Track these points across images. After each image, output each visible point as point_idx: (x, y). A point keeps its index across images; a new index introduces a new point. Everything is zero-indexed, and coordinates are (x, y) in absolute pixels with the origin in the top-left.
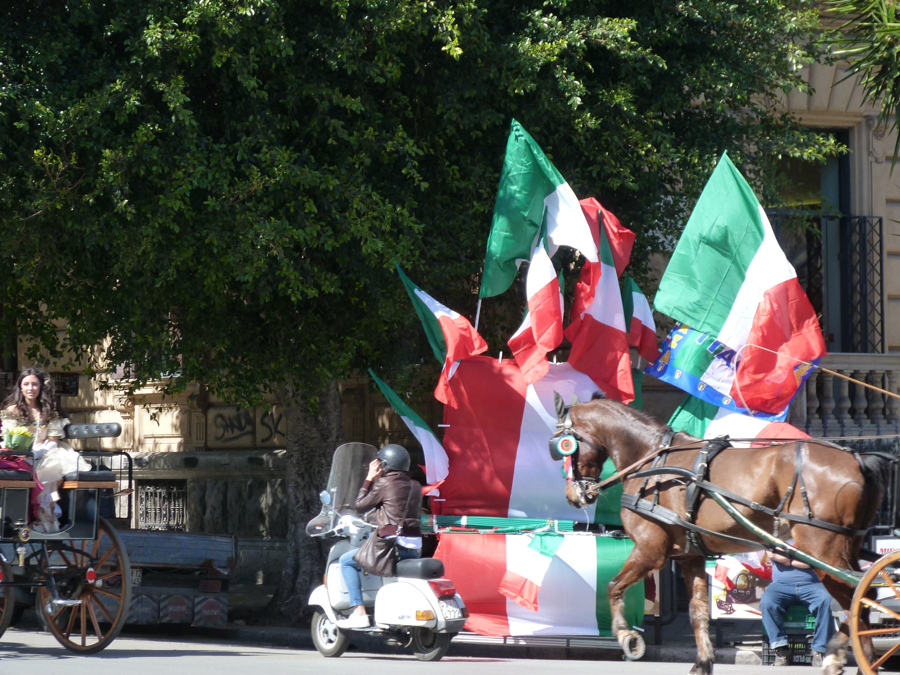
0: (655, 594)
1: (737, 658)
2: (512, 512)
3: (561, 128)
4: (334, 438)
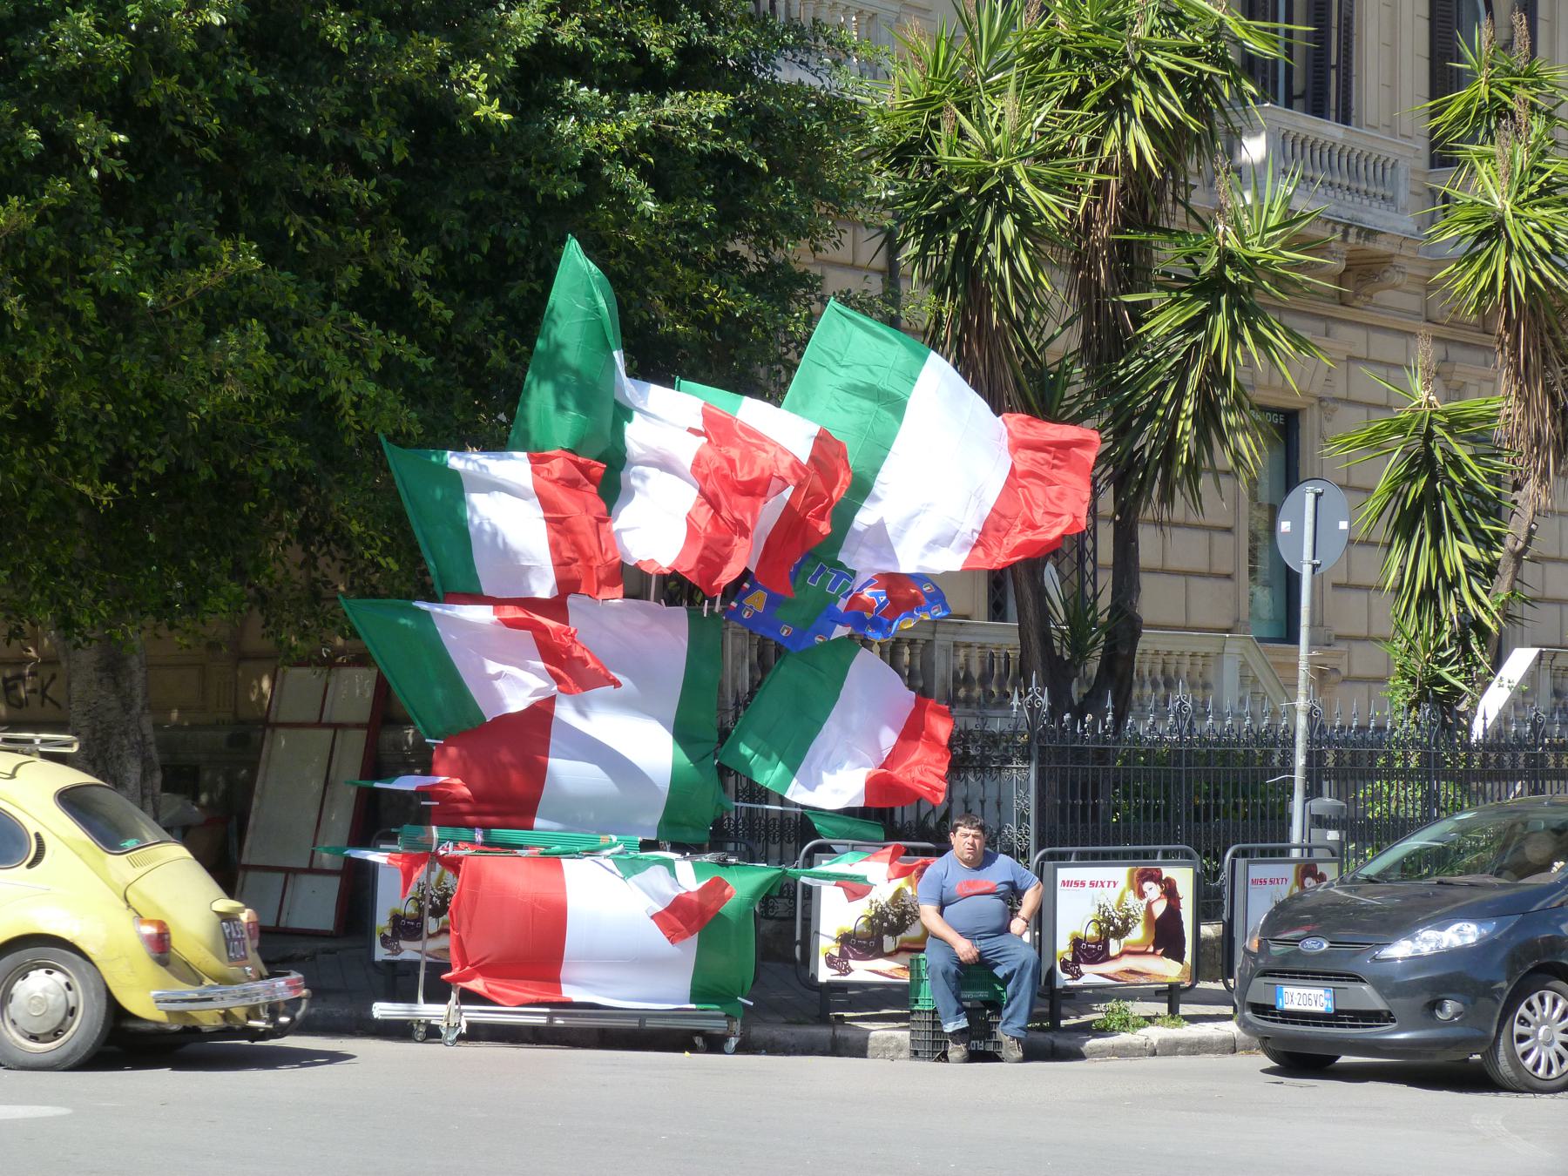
0: (1183, 953)
1: (871, 1043)
2: (538, 823)
3: (86, 130)
4: (138, 709)
